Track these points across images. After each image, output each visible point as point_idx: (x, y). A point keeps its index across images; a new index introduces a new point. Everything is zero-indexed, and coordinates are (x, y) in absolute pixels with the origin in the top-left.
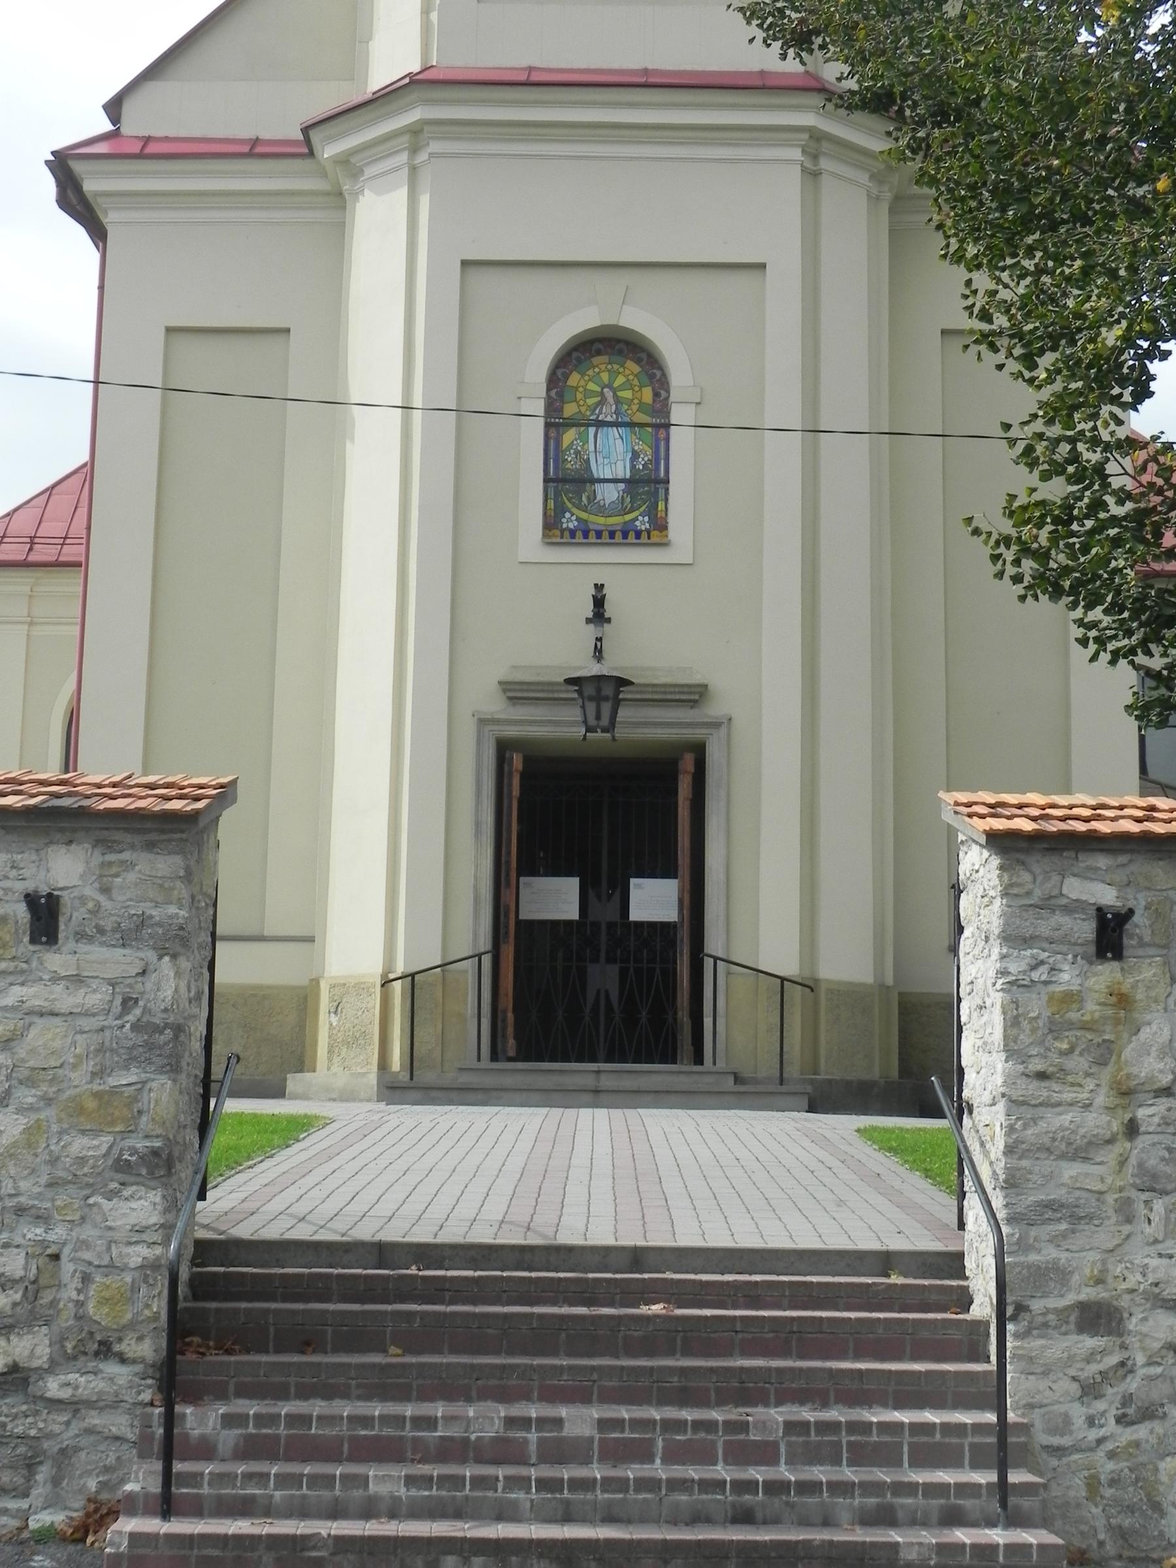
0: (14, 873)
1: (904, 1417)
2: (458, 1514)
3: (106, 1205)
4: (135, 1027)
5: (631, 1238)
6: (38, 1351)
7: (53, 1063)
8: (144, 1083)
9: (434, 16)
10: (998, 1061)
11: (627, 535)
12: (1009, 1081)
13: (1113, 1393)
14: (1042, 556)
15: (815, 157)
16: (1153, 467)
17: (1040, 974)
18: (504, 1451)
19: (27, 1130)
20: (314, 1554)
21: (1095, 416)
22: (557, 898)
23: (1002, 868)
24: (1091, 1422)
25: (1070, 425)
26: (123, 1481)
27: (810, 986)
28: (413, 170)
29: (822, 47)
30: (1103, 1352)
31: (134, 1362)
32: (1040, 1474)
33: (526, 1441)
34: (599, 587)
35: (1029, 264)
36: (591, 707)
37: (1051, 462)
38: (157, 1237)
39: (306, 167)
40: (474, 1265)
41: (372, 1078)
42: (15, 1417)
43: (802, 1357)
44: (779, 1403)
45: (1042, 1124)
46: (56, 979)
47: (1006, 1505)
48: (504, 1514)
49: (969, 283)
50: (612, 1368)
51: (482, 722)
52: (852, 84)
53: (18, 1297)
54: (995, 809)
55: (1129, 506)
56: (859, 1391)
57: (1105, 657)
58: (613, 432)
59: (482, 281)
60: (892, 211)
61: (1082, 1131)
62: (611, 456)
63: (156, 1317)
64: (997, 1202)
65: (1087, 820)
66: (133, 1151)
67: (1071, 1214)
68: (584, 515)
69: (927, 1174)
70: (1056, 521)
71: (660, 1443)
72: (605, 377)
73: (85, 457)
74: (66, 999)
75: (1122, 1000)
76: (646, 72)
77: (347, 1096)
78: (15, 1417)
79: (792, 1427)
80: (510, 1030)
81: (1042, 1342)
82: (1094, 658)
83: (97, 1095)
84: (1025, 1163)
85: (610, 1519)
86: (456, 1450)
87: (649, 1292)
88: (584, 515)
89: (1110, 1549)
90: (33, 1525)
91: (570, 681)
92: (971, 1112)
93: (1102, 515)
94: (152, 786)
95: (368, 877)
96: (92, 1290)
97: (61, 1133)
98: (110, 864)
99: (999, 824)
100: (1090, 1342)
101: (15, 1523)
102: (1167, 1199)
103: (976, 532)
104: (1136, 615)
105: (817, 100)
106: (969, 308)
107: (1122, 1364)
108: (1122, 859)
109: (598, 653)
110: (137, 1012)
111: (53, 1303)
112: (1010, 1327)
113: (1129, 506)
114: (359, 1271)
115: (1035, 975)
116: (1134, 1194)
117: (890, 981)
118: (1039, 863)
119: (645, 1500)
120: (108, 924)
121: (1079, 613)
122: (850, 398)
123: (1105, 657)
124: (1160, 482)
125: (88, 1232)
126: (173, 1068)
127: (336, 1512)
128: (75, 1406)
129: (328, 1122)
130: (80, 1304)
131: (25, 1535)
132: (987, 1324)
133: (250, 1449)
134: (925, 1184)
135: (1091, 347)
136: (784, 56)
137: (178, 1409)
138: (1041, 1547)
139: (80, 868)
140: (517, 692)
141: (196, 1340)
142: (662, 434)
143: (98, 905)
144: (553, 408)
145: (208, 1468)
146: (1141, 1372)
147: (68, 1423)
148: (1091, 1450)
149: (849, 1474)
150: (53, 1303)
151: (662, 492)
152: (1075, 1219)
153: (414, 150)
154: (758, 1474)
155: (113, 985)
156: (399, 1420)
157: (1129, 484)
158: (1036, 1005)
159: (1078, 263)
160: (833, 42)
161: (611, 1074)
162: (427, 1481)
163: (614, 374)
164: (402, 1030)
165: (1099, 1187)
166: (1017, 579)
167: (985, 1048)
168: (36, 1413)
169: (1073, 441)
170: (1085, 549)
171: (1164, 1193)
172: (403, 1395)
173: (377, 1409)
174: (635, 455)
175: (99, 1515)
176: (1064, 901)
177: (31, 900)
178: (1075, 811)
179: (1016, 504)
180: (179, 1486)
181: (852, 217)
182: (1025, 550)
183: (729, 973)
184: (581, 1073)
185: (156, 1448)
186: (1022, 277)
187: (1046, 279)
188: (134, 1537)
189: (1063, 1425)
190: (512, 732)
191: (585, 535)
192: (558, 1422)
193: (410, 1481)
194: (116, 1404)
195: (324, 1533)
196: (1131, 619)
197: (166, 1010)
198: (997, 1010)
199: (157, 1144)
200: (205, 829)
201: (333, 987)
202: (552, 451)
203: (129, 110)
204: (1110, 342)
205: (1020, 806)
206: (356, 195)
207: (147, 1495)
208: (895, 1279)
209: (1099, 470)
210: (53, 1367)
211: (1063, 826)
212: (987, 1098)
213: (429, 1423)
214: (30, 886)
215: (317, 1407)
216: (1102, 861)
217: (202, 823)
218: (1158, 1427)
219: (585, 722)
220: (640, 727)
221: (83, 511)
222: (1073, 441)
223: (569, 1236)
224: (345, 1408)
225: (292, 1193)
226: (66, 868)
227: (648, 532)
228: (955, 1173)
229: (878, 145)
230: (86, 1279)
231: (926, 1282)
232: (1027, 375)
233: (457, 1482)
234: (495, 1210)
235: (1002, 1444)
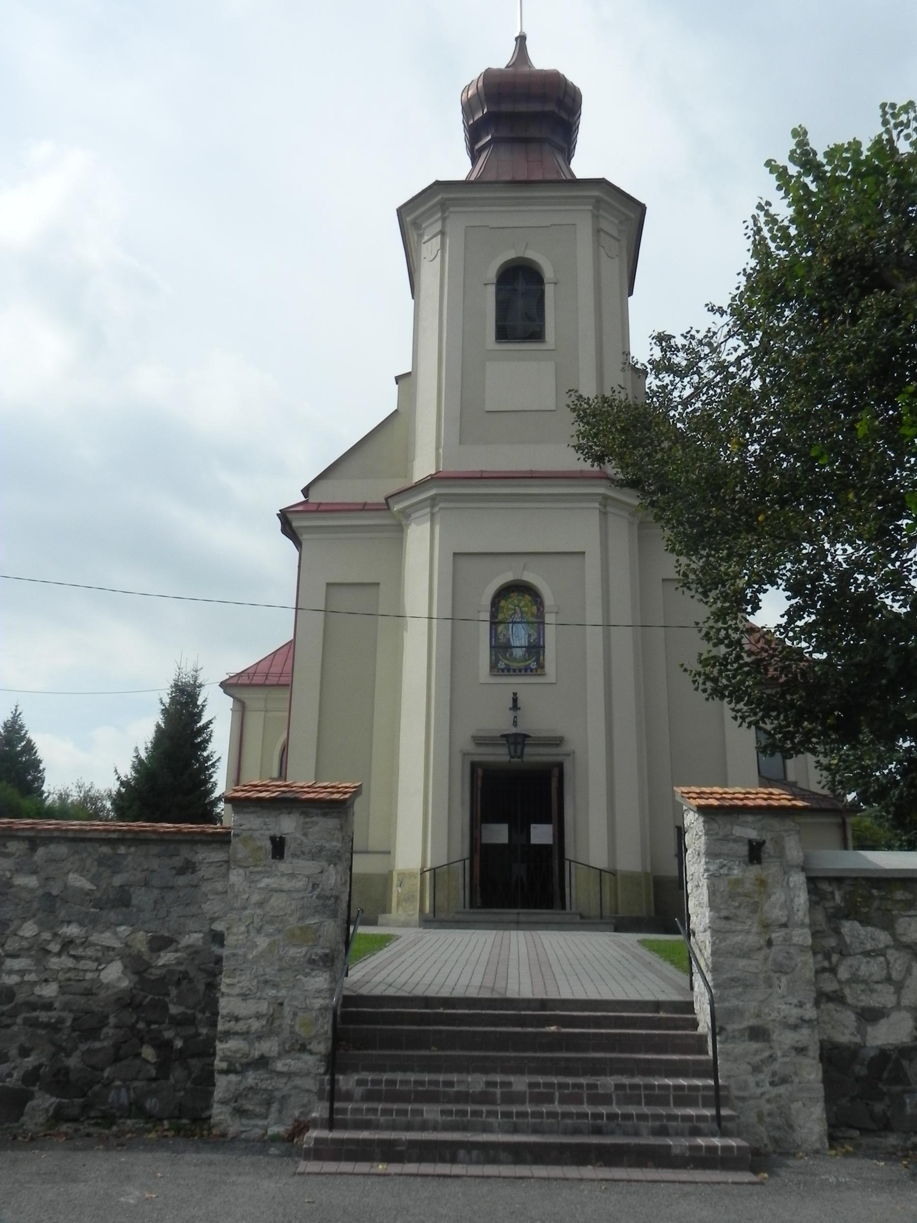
0: (265, 827)
1: (669, 1082)
2: (464, 1128)
3: (304, 979)
4: (318, 897)
5: (540, 995)
6: (273, 1048)
7: (281, 913)
8: (322, 922)
9: (441, 451)
10: (707, 912)
11: (526, 671)
12: (712, 921)
13: (767, 1070)
14: (715, 680)
15: (605, 506)
16: (762, 641)
17: (724, 871)
18: (484, 1098)
19: (269, 945)
20: (399, 1148)
21: (736, 618)
22: (498, 834)
23: (704, 822)
24: (758, 1084)
25: (725, 622)
26: (310, 1111)
27: (613, 873)
28: (433, 515)
29: (609, 461)
30: (762, 1051)
31: (316, 1054)
32: (735, 1110)
33: (494, 1094)
34: (515, 694)
35: (704, 553)
36: (512, 748)
37: (718, 638)
38: (327, 994)
40: (468, 1007)
41: (417, 916)
42: (262, 1080)
43: (621, 1051)
44: (611, 1074)
45: (728, 941)
46: (283, 875)
47: (721, 1126)
48: (486, 1129)
49: (678, 561)
50: (534, 1058)
51: (465, 754)
52: (620, 476)
53: (264, 1022)
54: (700, 795)
55: (753, 658)
56: (649, 1069)
57: (745, 725)
58: (520, 626)
60: (639, 528)
61: (747, 944)
62: (520, 636)
63: (326, 1032)
64: (709, 977)
65: (742, 799)
66: (317, 954)
68: (507, 662)
69: (672, 962)
70: (721, 664)
71: (557, 1094)
72: (516, 602)
73: (292, 638)
74: (287, 884)
75: (762, 883)
76: (531, 472)
77: (406, 925)
78: (262, 1080)
79: (618, 1087)
80: (478, 894)
81: (733, 1045)
82: (740, 725)
83: (301, 928)
84: (721, 960)
85: (535, 1131)
86: (462, 1097)
87: (549, 1021)
88: (507, 662)
89: (770, 1148)
90: (269, 1133)
91: (502, 736)
92: (694, 935)
93: (741, 662)
94: (325, 788)
95: (414, 825)
96: (298, 1019)
97: (284, 946)
98: (307, 823)
99: (702, 802)
100: (755, 1045)
101: (261, 1132)
102: (788, 977)
103: (685, 670)
104: (758, 706)
105: (608, 483)
106: (678, 572)
107: (771, 1056)
108: (759, 817)
109: (515, 723)
110: (319, 890)
111: (280, 1026)
112: (718, 1038)
113: (753, 658)
114: (416, 1010)
115: (722, 871)
116: (772, 974)
117: (649, 870)
118: (721, 820)
119: (551, 1123)
120: (306, 850)
121: (733, 705)
122: (623, 612)
123: (745, 725)
124: (766, 647)
125: (296, 992)
126: (334, 915)
127: (409, 1127)
128: (289, 1075)
129: (397, 938)
130: (292, 1026)
131: (266, 1138)
132: (706, 1036)
133: (369, 1096)
134: (671, 968)
135: (732, 588)
136: (593, 466)
137: (337, 1077)
138: (739, 1148)
139: (294, 824)
140: (480, 741)
141: (344, 1043)
142: (541, 626)
143: (302, 841)
144: (494, 615)
145: (350, 1106)
146: (781, 1060)
147: (286, 1083)
148: (759, 1098)
149: (646, 1110)
150: (280, 1026)
151: (542, 652)
152: (746, 986)
153: (433, 506)
154: (603, 1110)
155: (308, 878)
156: (436, 1083)
157: (754, 649)
158: (723, 886)
159: (725, 552)
160: (614, 459)
161: (524, 914)
162: (450, 1113)
163: (520, 601)
165: (755, 971)
166: (705, 691)
167: (700, 905)
168: (272, 1078)
169: (726, 629)
170: (734, 677)
171: (786, 973)
172: (437, 1070)
173: (426, 1077)
174: (530, 636)
175: (300, 1128)
176: (733, 837)
177: (273, 839)
178: (736, 795)
179: (703, 658)
180: (337, 1114)
181: (622, 533)
182: (708, 678)
183: (576, 868)
184: (511, 914)
185: (326, 1095)
186: (701, 558)
187: (711, 559)
188: (317, 1140)
189: (745, 1087)
190: (477, 759)
191: (508, 671)
192: (510, 1084)
193: (443, 1112)
194: (308, 1074)
195: (404, 1138)
196: (756, 708)
197: (331, 889)
198: (705, 887)
199: (327, 951)
200: (348, 807)
201: (398, 874)
202: (493, 634)
203: (312, 493)
204: (741, 586)
205: (711, 793)
206: (408, 525)
207: (322, 1119)
208: (662, 1014)
209: (739, 642)
210: (280, 1056)
211: (731, 803)
212: (702, 928)
213: (450, 1084)
214: (272, 833)
215: (399, 1076)
216: (750, 818)
217: (348, 803)
218: (789, 1087)
219: (510, 754)
220: (534, 755)
221: (290, 662)
222: (726, 629)
223: (512, 994)
224: (412, 1077)
225: (384, 973)
226: (288, 825)
227: (536, 669)
228: (685, 962)
229: (636, 502)
230: (295, 1014)
231: (676, 1016)
232: (705, 600)
233: (464, 1113)
234: (477, 981)
235: (717, 1096)
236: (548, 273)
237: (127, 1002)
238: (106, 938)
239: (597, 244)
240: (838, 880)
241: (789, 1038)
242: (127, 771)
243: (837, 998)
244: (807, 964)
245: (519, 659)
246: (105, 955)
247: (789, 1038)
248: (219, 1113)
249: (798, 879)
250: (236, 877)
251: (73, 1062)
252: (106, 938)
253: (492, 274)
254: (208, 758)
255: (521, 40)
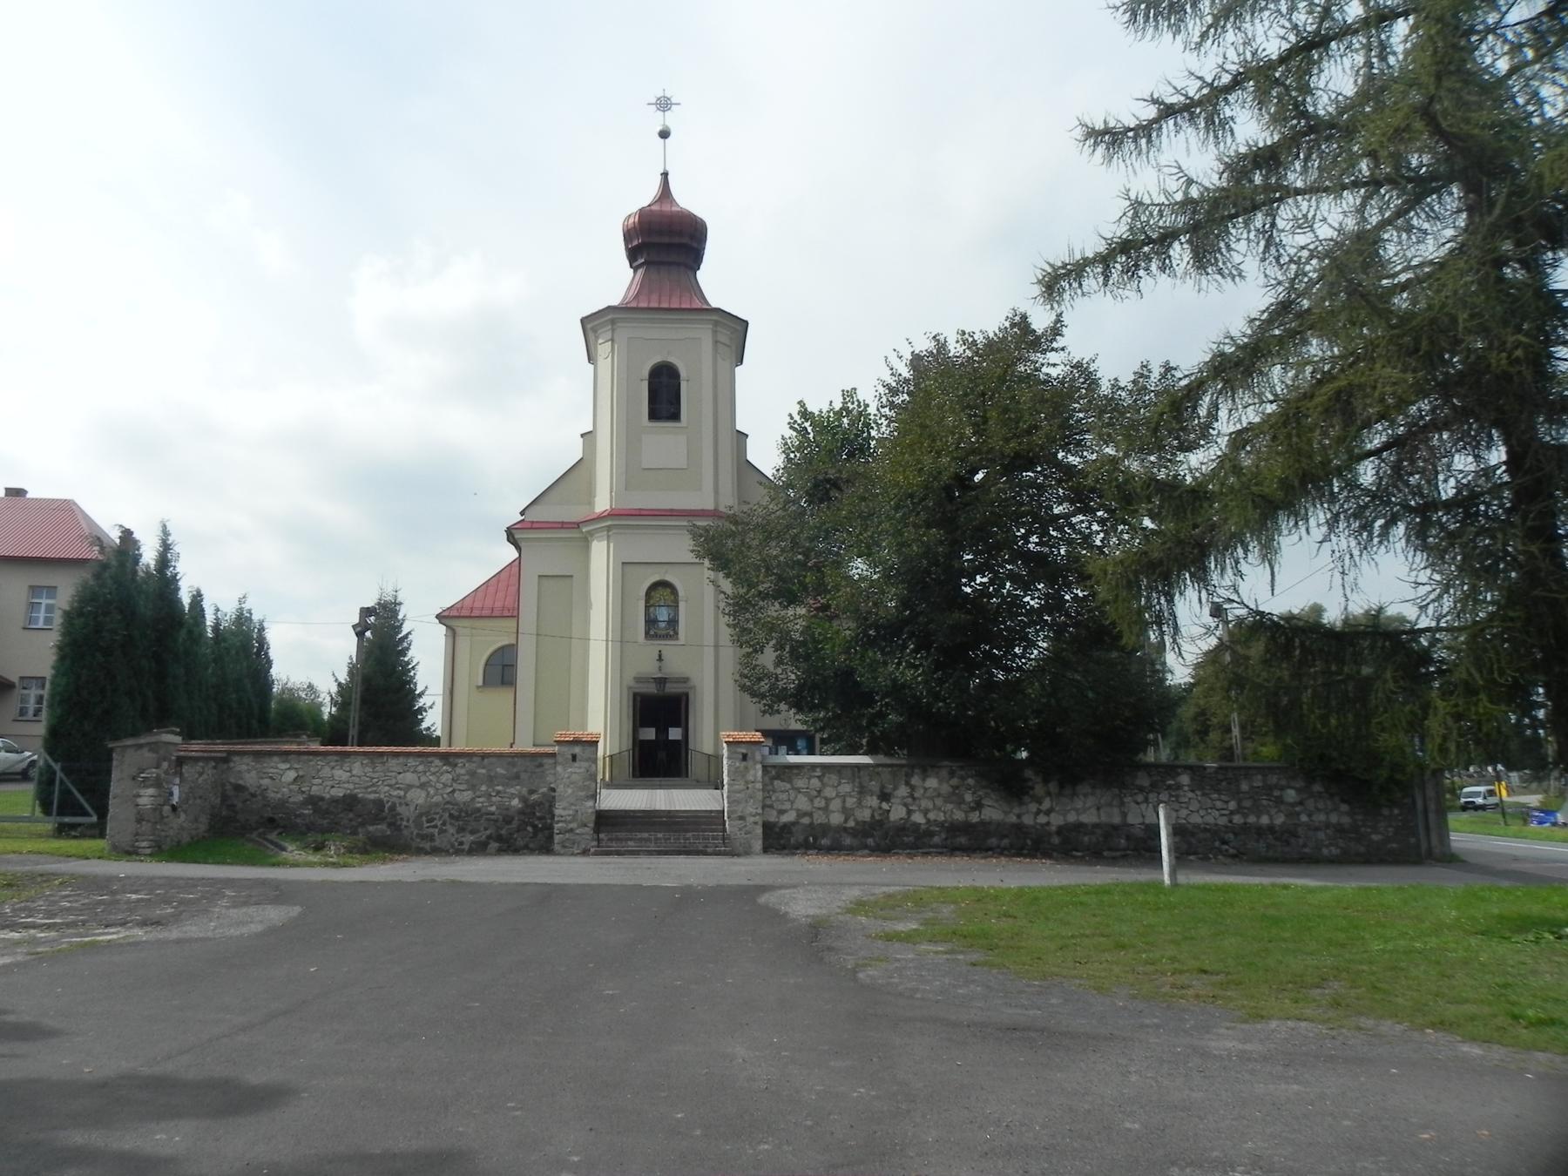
11: (667, 637)
22: (649, 734)
39: (577, 532)
51: (629, 688)
59: (629, 568)
67: (738, 802)
140: (638, 680)
164: (1284, 875)
184: (657, 780)
191: (657, 637)
220: (671, 689)
226: (577, 750)
236: (683, 374)
237: (521, 812)
238: (512, 790)
239: (715, 350)
240: (774, 767)
241: (752, 819)
242: (343, 677)
243: (771, 807)
244: (760, 795)
245: (661, 627)
246: (512, 796)
247: (752, 819)
248: (557, 847)
249: (759, 766)
250: (559, 769)
251: (503, 832)
252: (512, 790)
253: (646, 374)
254: (408, 663)
255: (665, 175)
